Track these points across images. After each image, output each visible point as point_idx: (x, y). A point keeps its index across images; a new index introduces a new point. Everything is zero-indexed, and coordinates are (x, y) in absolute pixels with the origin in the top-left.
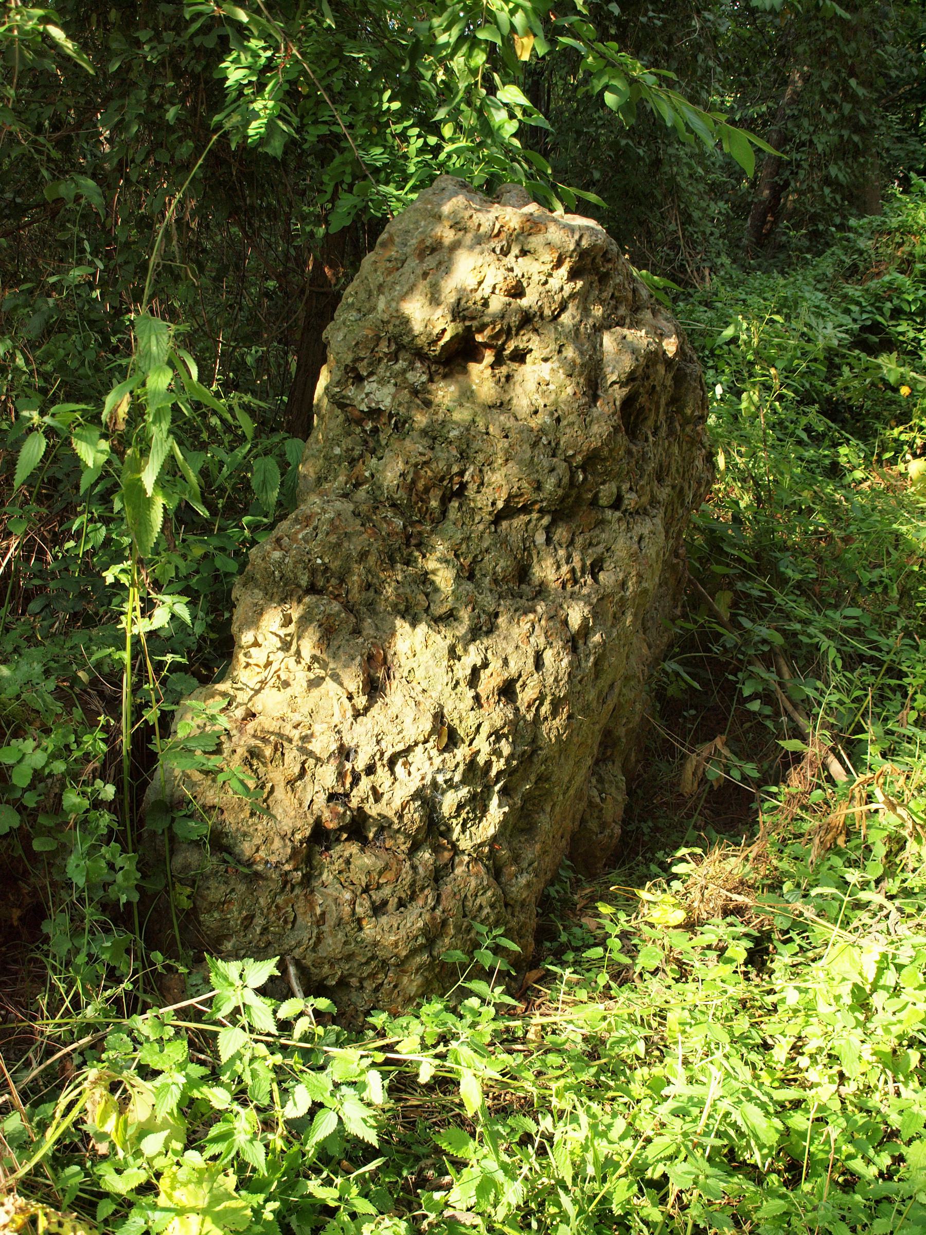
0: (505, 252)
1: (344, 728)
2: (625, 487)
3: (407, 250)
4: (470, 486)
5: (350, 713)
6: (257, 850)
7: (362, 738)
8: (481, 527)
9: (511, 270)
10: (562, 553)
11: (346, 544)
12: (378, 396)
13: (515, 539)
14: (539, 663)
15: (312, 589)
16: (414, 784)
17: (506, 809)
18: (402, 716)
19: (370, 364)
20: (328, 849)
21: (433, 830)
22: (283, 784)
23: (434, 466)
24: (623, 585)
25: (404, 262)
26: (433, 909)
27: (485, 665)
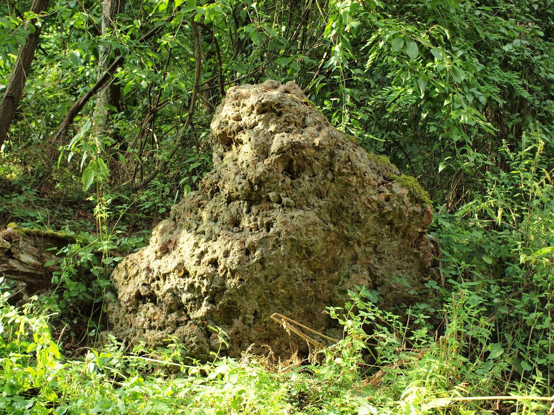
1: (151, 262)
7: (154, 265)
10: (253, 217)
17: (209, 308)
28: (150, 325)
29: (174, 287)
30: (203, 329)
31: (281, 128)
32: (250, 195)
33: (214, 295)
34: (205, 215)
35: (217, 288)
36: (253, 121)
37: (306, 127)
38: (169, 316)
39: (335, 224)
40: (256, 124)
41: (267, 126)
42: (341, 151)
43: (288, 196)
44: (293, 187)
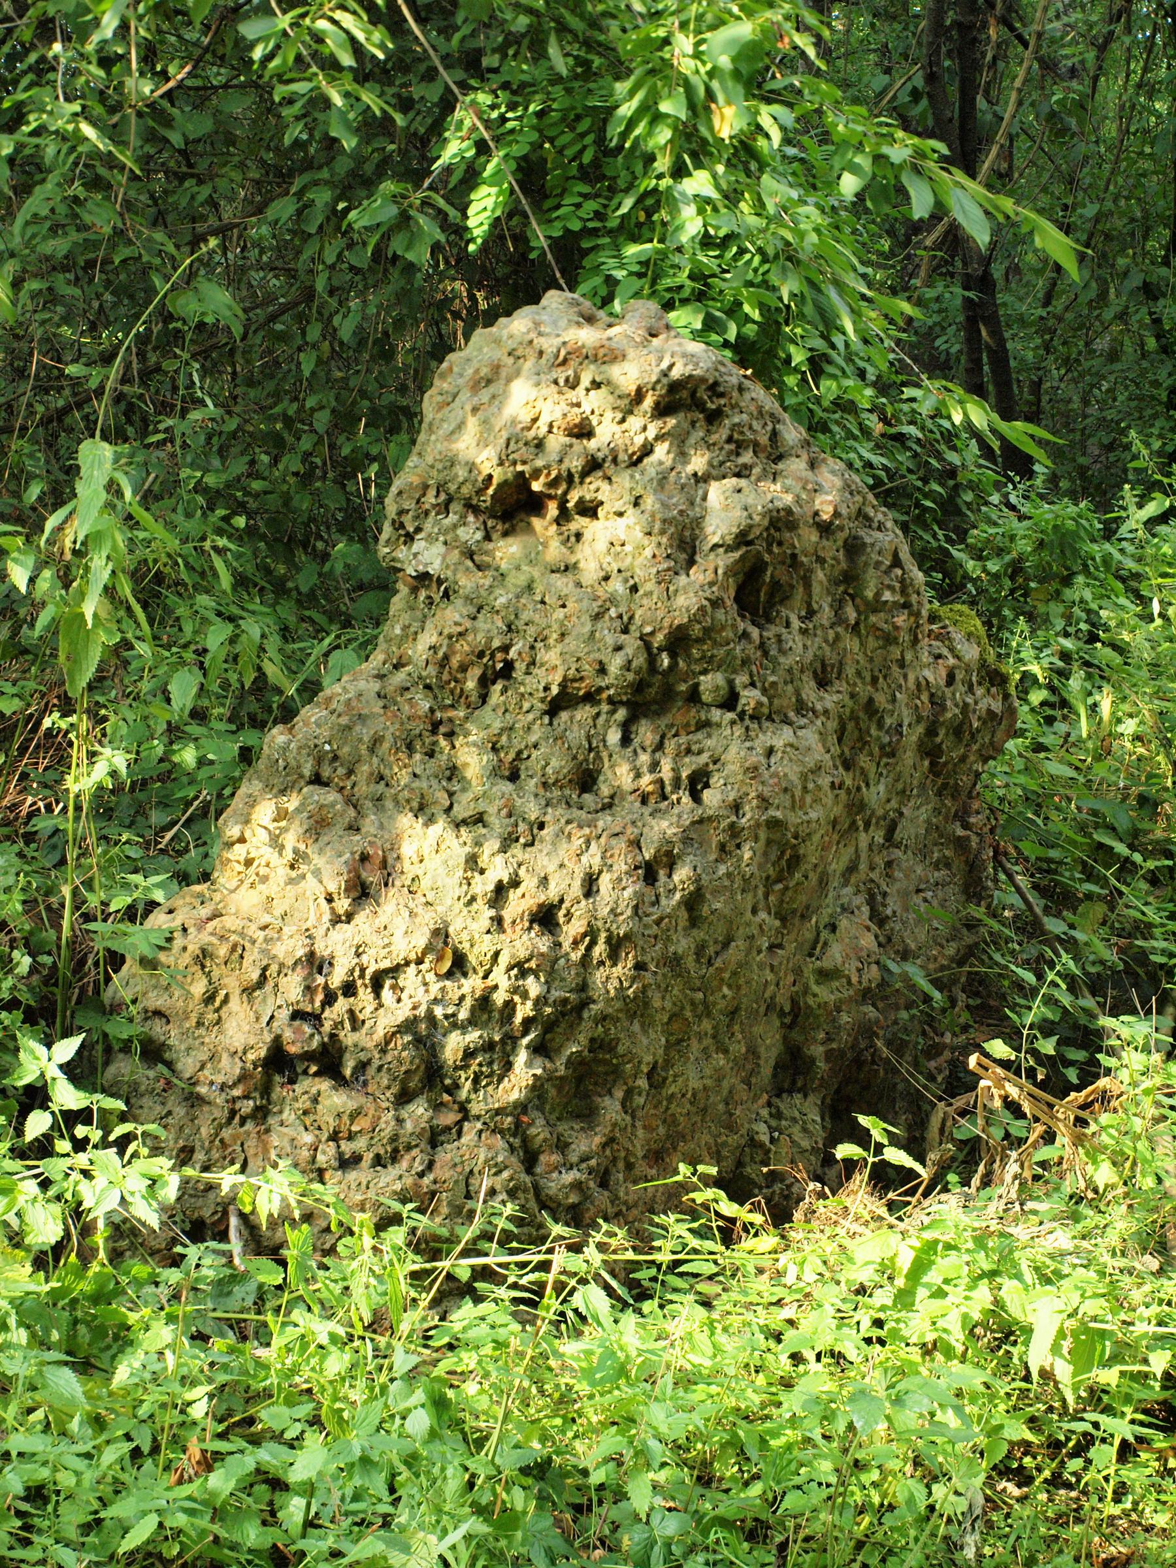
0: (572, 384)
1: (319, 933)
2: (741, 679)
3: (460, 381)
4: (517, 665)
5: (327, 917)
6: (202, 1068)
7: (338, 945)
8: (530, 717)
9: (578, 405)
10: (644, 758)
11: (358, 728)
12: (426, 557)
13: (576, 735)
14: (590, 885)
15: (317, 780)
16: (402, 1013)
17: (539, 1072)
18: (392, 929)
19: (417, 517)
20: (292, 1081)
22: (238, 991)
23: (470, 638)
24: (736, 807)
25: (455, 396)
26: (421, 1175)
27: (515, 883)
28: (341, 1155)
29: (422, 1011)
30: (517, 1142)
31: (722, 463)
32: (639, 687)
34: (472, 759)
35: (565, 1001)
36: (639, 440)
37: (780, 458)
38: (404, 1114)
39: (848, 765)
40: (647, 450)
41: (682, 455)
42: (878, 535)
43: (753, 684)
44: (766, 654)
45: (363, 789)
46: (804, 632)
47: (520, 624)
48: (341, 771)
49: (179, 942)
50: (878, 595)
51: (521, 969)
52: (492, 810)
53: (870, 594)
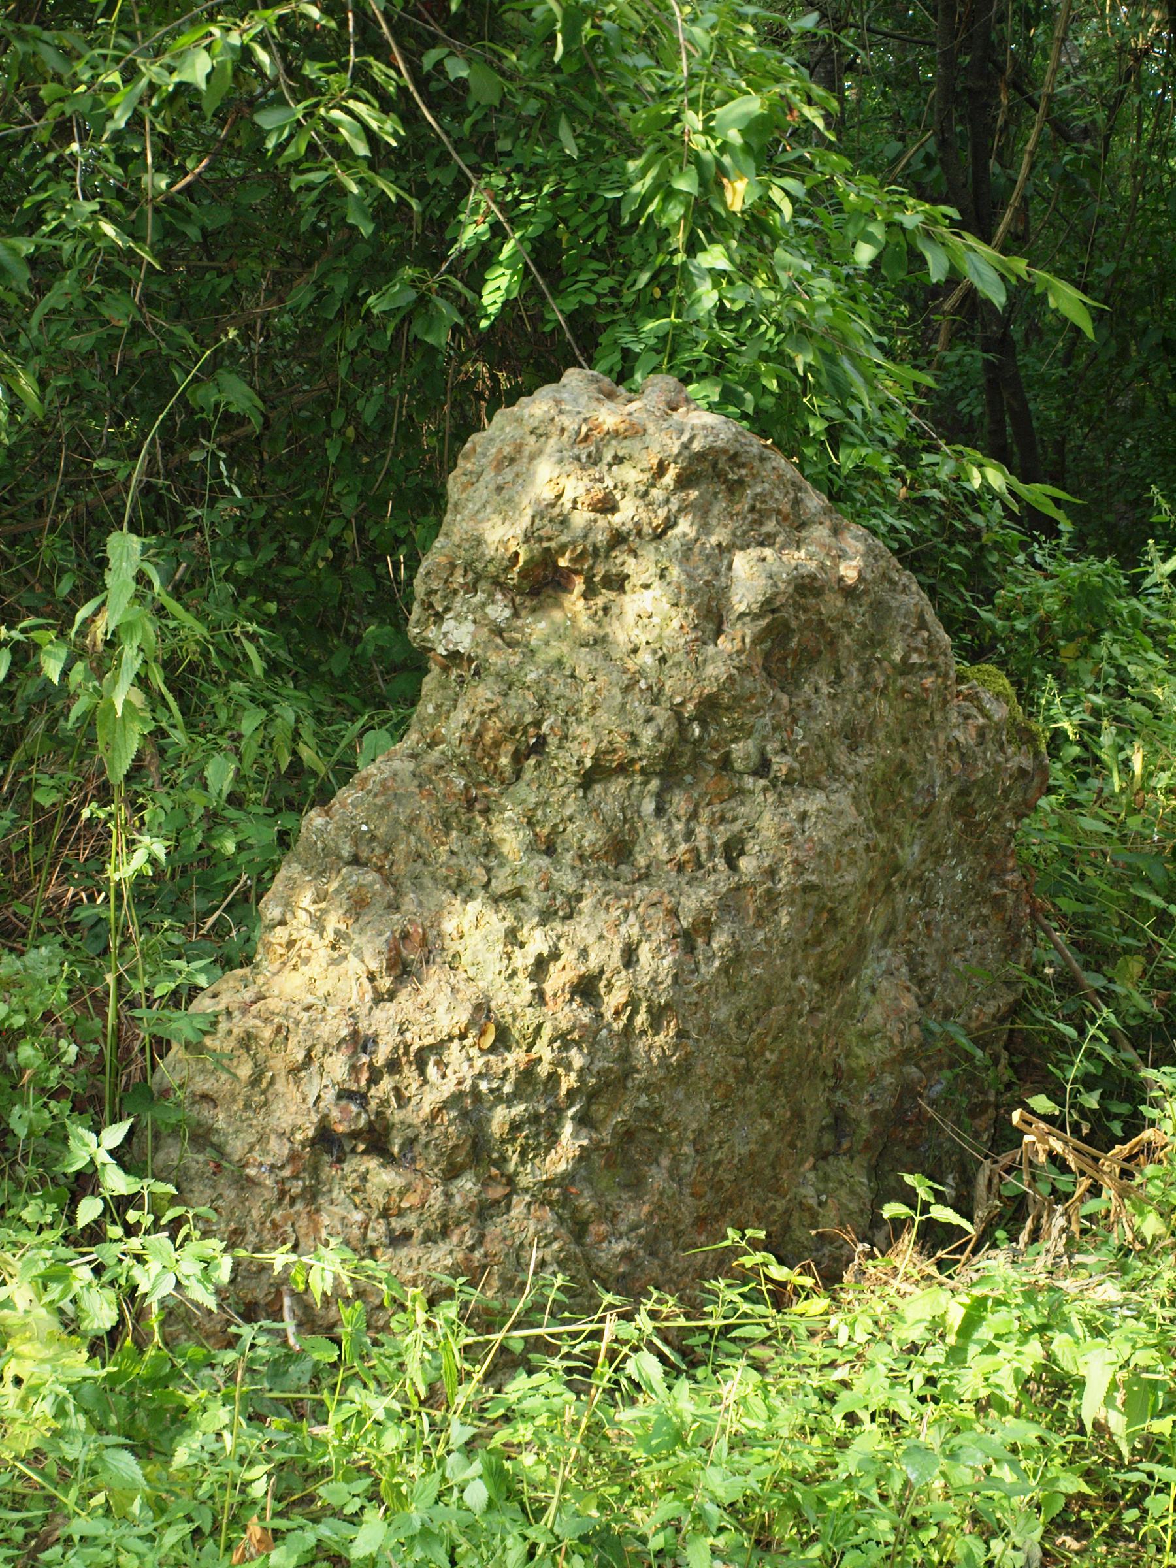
1: (362, 1011)
4: (550, 739)
5: (369, 996)
7: (382, 1023)
8: (565, 790)
10: (679, 827)
11: (394, 808)
13: (611, 807)
14: (630, 956)
16: (448, 1088)
19: (445, 597)
20: (340, 1160)
21: (476, 1153)
23: (503, 714)
26: (472, 1249)
27: (555, 955)
28: (391, 1231)
29: (467, 1086)
30: (566, 1214)
32: (669, 757)
33: (598, 1093)
34: (511, 840)
35: (610, 1070)
36: (662, 513)
37: (802, 526)
41: (705, 528)
45: (401, 868)
46: (833, 697)
47: (551, 699)
48: (378, 851)
49: (223, 1026)
50: (905, 659)
51: (563, 1040)
52: (530, 884)
53: (897, 657)
